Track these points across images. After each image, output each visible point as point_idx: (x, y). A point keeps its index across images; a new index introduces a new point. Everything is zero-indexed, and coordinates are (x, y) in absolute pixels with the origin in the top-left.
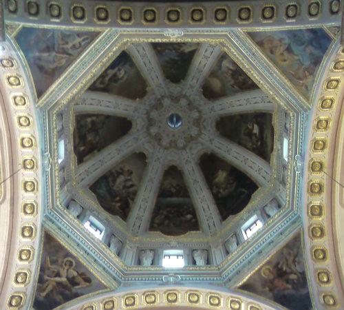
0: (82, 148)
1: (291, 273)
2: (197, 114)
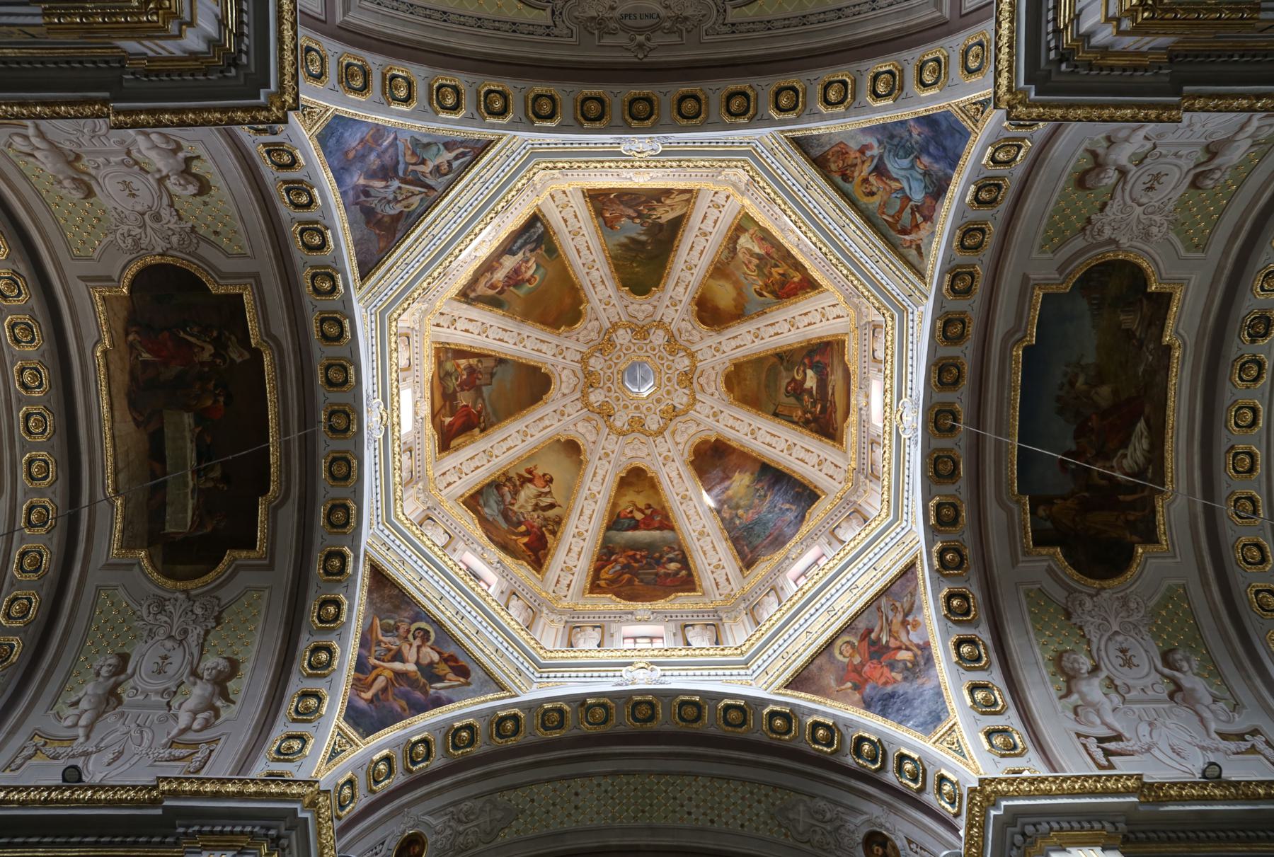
0: (448, 420)
1: (900, 648)
2: (687, 362)
